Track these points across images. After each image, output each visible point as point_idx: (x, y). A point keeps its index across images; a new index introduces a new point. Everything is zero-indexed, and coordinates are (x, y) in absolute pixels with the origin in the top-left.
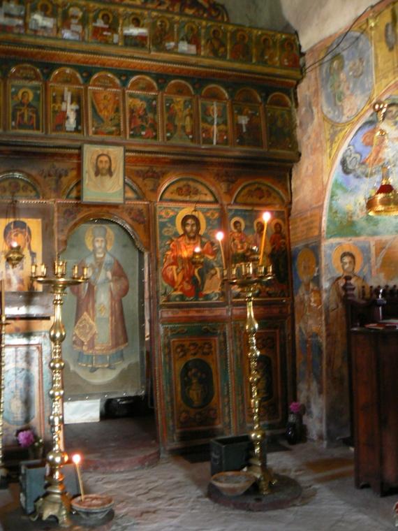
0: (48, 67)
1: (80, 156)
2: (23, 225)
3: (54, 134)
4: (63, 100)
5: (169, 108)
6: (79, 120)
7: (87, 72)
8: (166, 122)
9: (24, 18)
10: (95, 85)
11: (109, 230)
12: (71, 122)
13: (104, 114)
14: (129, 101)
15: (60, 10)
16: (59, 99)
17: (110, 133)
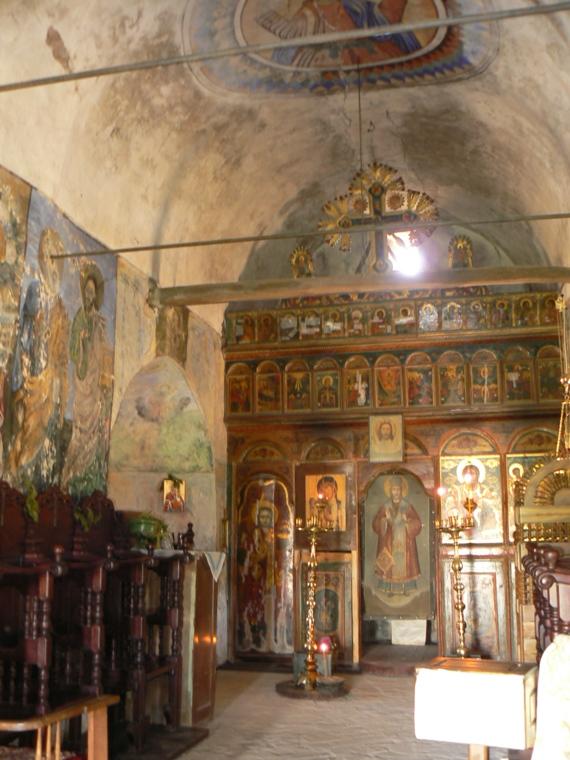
0: (342, 357)
1: (366, 425)
2: (331, 480)
3: (350, 409)
4: (355, 381)
5: (442, 376)
6: (367, 396)
7: (372, 356)
8: (440, 388)
9: (320, 326)
10: (379, 366)
11: (404, 480)
12: (362, 398)
13: (388, 388)
14: (409, 375)
15: (346, 315)
16: (352, 381)
17: (394, 403)
